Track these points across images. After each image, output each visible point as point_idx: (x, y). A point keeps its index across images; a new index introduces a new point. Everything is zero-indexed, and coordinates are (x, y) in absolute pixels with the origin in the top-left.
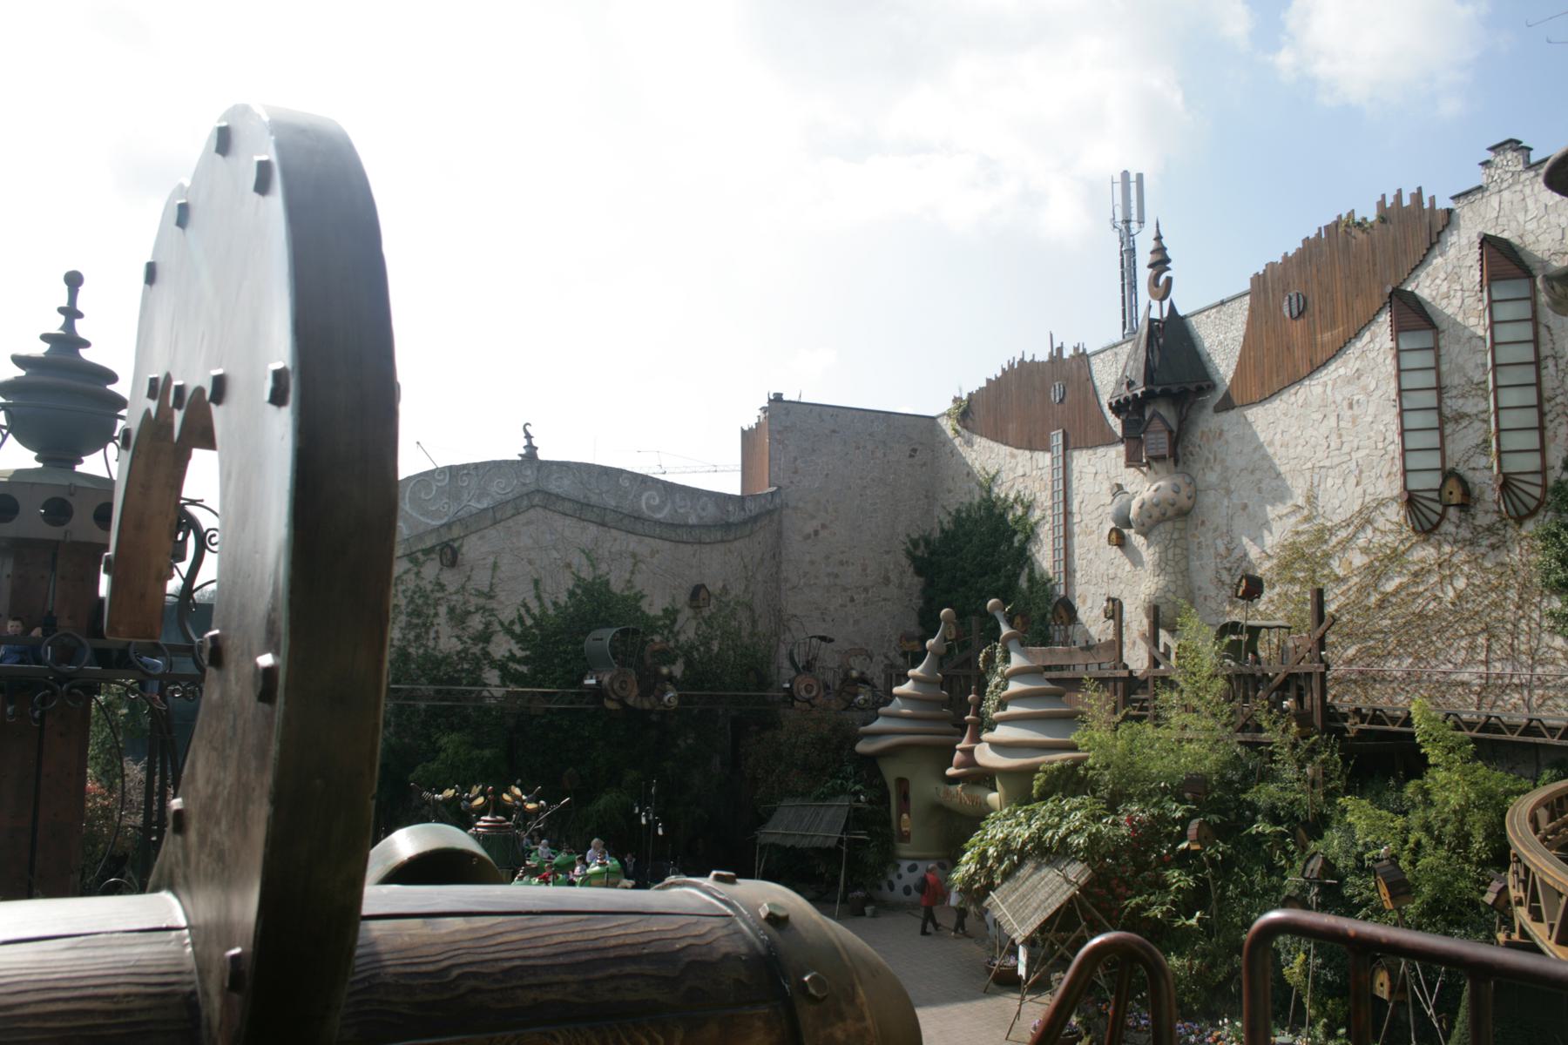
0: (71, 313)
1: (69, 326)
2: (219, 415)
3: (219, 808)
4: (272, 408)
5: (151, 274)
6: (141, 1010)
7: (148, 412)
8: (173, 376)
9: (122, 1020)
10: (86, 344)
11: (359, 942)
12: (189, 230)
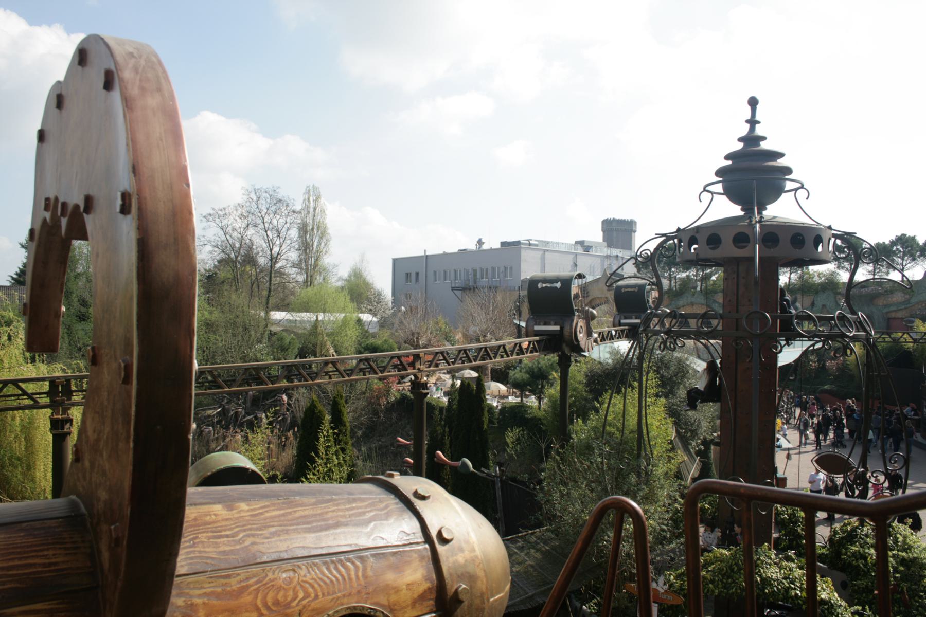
0: (753, 122)
1: (752, 129)
2: (89, 220)
3: (101, 447)
4: (121, 216)
5: (42, 136)
6: (63, 562)
7: (45, 220)
8: (59, 197)
9: (53, 568)
10: (764, 138)
11: (185, 520)
12: (63, 111)
